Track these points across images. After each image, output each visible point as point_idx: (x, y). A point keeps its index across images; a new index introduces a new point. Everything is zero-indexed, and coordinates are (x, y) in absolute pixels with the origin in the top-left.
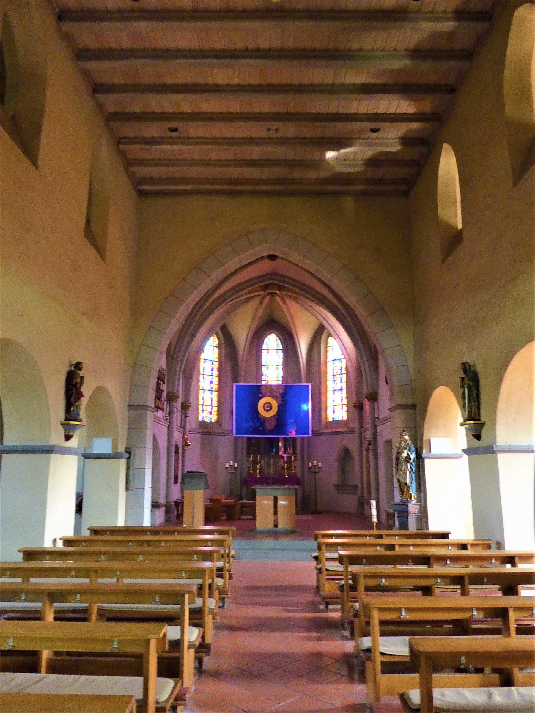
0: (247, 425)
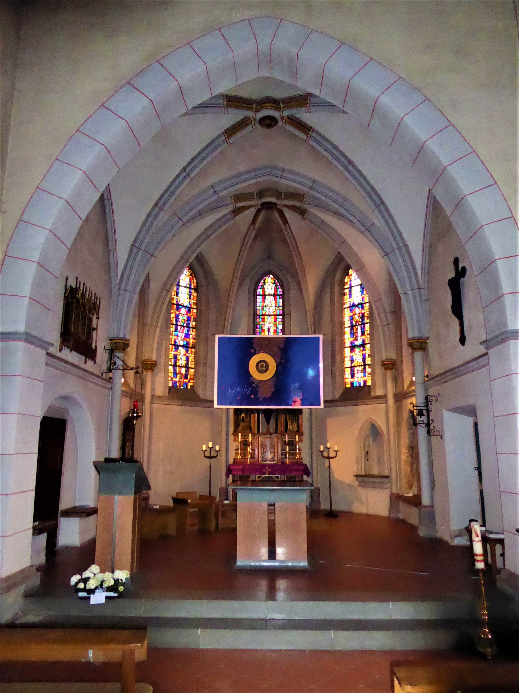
0: (233, 391)
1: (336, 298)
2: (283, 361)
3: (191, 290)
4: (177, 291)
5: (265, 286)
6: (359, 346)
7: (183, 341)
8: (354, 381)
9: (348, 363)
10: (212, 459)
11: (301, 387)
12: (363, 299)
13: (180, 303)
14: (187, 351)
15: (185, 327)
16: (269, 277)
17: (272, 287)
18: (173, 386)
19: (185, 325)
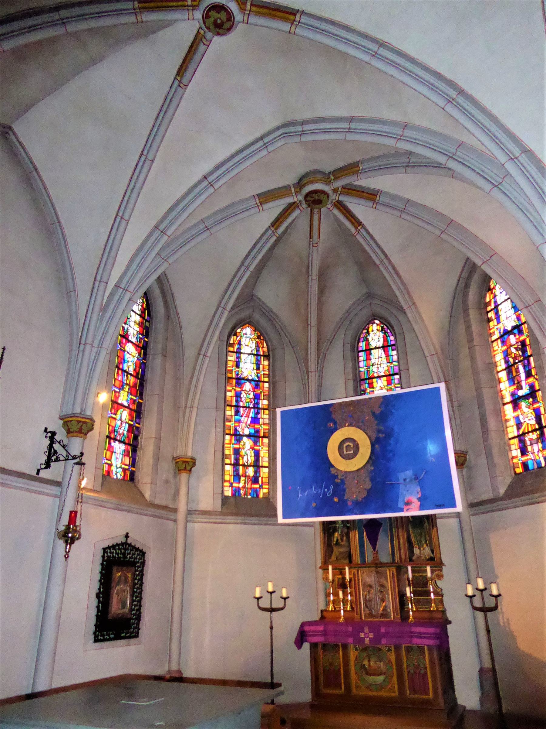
0: (306, 494)
1: (475, 327)
2: (381, 436)
3: (259, 357)
4: (237, 360)
5: (370, 338)
6: (525, 397)
7: (249, 428)
8: (528, 460)
9: (512, 431)
10: (273, 613)
11: (416, 478)
12: (518, 318)
13: (242, 377)
14: (255, 443)
15: (252, 408)
16: (374, 323)
17: (379, 336)
18: (234, 494)
19: (251, 406)
